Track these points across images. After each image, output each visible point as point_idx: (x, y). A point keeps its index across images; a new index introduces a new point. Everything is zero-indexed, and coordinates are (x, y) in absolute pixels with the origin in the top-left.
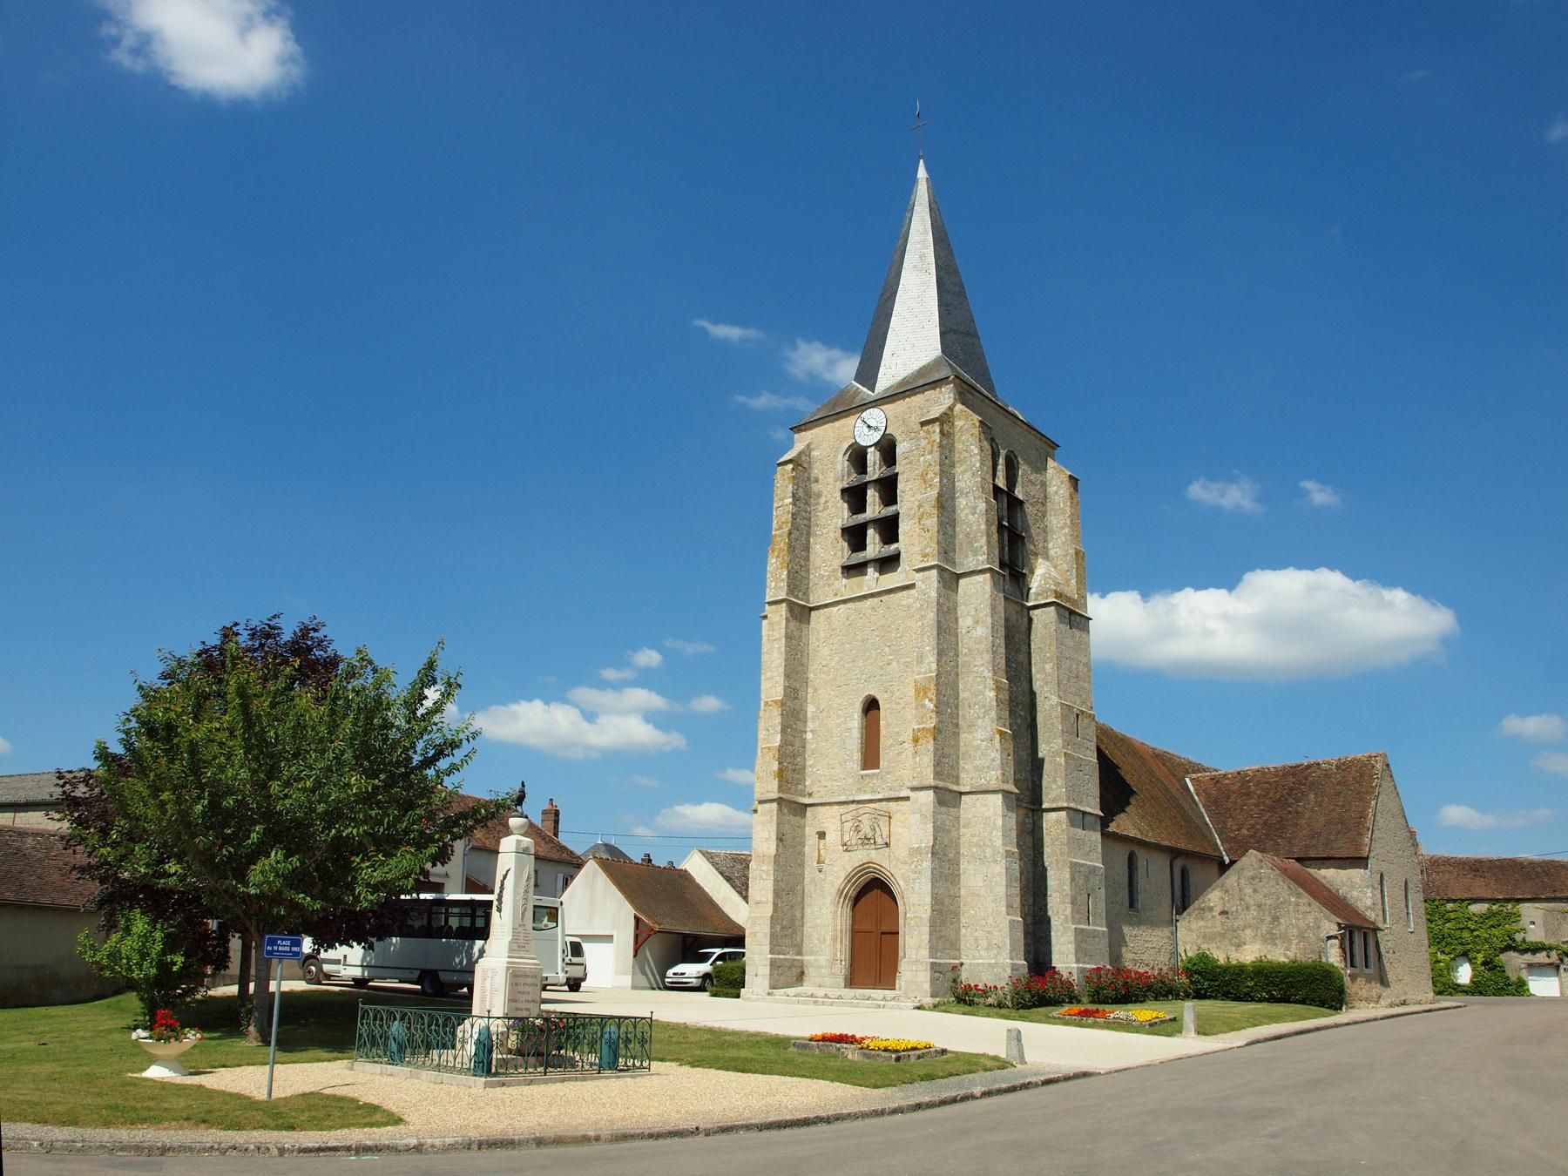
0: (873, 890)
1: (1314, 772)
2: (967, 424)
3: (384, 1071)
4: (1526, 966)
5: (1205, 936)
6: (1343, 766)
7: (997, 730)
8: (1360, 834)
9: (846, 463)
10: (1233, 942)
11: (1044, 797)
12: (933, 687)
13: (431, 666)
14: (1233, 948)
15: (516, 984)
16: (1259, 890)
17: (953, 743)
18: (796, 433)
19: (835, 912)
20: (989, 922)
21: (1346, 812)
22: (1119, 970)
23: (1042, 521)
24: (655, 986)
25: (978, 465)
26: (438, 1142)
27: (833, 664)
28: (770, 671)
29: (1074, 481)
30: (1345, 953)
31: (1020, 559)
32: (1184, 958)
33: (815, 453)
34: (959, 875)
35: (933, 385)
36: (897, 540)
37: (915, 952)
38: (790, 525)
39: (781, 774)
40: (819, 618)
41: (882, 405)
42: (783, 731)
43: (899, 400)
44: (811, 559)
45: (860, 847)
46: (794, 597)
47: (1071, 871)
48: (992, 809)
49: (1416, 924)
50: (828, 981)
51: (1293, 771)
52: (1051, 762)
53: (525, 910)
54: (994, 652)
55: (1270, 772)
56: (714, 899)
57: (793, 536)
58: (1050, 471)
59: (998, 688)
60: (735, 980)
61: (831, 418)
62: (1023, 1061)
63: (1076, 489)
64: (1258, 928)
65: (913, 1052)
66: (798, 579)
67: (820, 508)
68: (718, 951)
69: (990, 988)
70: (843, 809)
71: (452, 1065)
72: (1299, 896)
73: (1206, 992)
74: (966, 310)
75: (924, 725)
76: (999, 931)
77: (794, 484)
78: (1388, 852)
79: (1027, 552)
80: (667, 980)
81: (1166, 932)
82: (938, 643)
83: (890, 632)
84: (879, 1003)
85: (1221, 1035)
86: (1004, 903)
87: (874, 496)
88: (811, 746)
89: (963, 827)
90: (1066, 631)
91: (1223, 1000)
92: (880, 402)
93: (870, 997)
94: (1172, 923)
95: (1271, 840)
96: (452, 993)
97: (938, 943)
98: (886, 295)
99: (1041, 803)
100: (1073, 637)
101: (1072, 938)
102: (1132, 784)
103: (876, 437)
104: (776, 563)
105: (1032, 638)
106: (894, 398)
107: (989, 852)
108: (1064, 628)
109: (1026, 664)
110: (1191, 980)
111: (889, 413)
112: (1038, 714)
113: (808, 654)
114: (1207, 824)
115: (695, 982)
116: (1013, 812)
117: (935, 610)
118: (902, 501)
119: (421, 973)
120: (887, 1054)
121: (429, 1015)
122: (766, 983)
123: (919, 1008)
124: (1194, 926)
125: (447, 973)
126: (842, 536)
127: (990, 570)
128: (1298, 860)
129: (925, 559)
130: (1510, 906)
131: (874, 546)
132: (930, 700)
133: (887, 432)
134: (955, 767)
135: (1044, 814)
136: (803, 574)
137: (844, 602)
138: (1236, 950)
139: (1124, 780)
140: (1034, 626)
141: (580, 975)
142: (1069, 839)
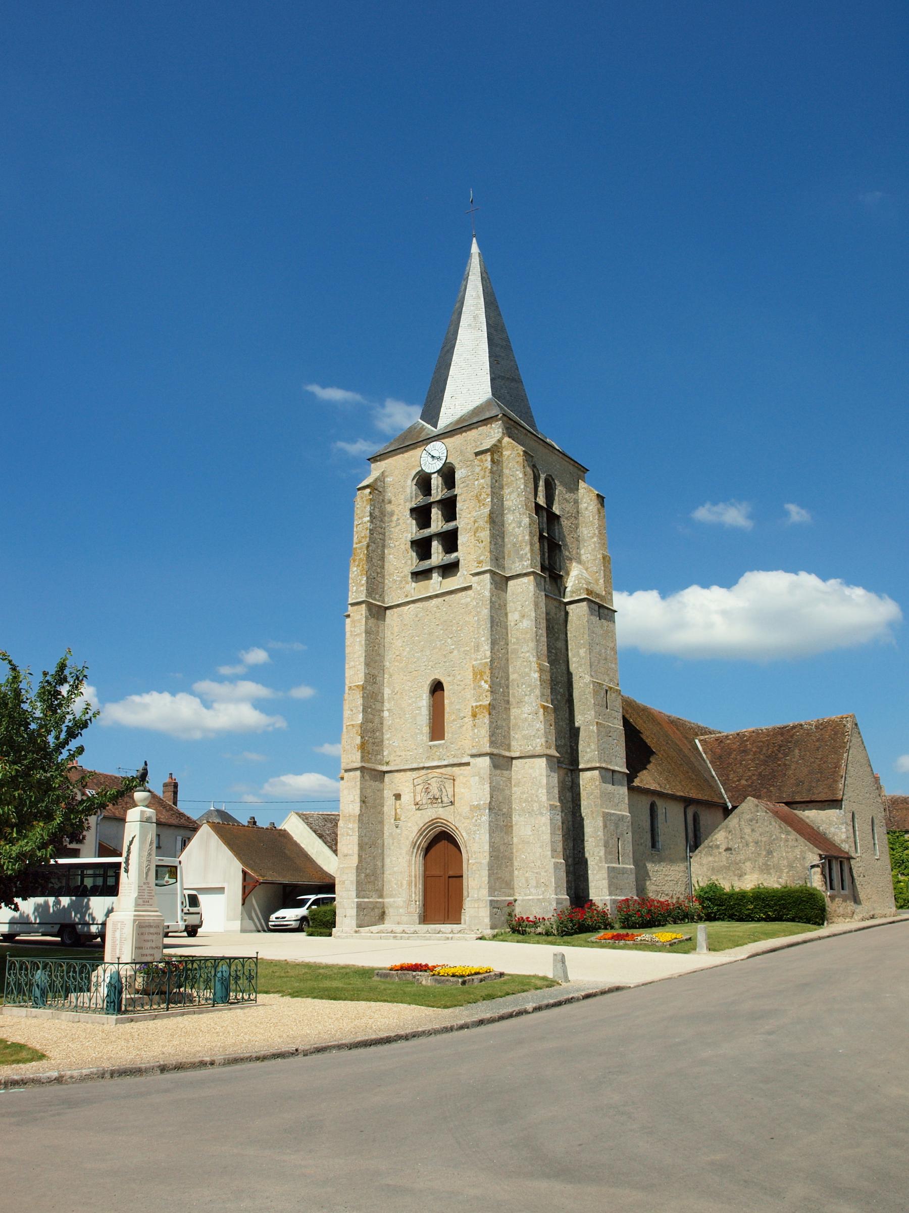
1: (798, 732)
2: (513, 453)
6: (821, 726)
8: (836, 781)
9: (414, 487)
10: (736, 872)
11: (580, 759)
12: (488, 672)
13: (62, 667)
14: (736, 878)
15: (142, 934)
16: (756, 829)
17: (505, 716)
19: (410, 861)
20: (537, 864)
22: (644, 900)
23: (576, 532)
24: (260, 929)
25: (522, 487)
26: (76, 1073)
27: (405, 653)
28: (353, 660)
29: (601, 498)
31: (558, 564)
32: (697, 888)
33: (389, 479)
34: (512, 826)
35: (485, 422)
38: (368, 539)
39: (363, 747)
41: (443, 438)
43: (457, 434)
44: (386, 567)
45: (430, 806)
46: (373, 599)
47: (604, 820)
48: (537, 771)
49: (881, 852)
50: (405, 919)
53: (149, 870)
54: (537, 641)
55: (763, 733)
57: (370, 548)
59: (541, 670)
60: (328, 921)
61: (401, 450)
62: (567, 980)
64: (756, 861)
65: (476, 977)
66: (375, 584)
67: (393, 524)
68: (313, 897)
69: (539, 919)
70: (415, 774)
72: (788, 833)
73: (715, 915)
74: (511, 360)
75: (481, 703)
76: (545, 872)
78: (858, 795)
81: (682, 866)
82: (491, 635)
86: (549, 848)
87: (437, 513)
88: (388, 722)
91: (729, 921)
93: (440, 931)
94: (687, 859)
97: (495, 883)
100: (602, 627)
101: (606, 875)
102: (652, 746)
103: (438, 465)
105: (568, 628)
106: (453, 433)
107: (536, 806)
108: (595, 619)
109: (563, 651)
110: (703, 906)
111: (450, 446)
112: (574, 690)
113: (384, 646)
114: (713, 777)
115: (294, 924)
116: (555, 772)
117: (489, 607)
118: (460, 518)
120: (455, 979)
122: (354, 923)
123: (480, 939)
124: (704, 861)
126: (412, 547)
127: (533, 573)
128: (787, 804)
129: (480, 565)
131: (438, 555)
132: (485, 682)
133: (447, 461)
134: (507, 736)
135: (581, 773)
136: (379, 579)
137: (413, 602)
138: (739, 879)
139: (645, 743)
140: (570, 618)
141: (197, 922)
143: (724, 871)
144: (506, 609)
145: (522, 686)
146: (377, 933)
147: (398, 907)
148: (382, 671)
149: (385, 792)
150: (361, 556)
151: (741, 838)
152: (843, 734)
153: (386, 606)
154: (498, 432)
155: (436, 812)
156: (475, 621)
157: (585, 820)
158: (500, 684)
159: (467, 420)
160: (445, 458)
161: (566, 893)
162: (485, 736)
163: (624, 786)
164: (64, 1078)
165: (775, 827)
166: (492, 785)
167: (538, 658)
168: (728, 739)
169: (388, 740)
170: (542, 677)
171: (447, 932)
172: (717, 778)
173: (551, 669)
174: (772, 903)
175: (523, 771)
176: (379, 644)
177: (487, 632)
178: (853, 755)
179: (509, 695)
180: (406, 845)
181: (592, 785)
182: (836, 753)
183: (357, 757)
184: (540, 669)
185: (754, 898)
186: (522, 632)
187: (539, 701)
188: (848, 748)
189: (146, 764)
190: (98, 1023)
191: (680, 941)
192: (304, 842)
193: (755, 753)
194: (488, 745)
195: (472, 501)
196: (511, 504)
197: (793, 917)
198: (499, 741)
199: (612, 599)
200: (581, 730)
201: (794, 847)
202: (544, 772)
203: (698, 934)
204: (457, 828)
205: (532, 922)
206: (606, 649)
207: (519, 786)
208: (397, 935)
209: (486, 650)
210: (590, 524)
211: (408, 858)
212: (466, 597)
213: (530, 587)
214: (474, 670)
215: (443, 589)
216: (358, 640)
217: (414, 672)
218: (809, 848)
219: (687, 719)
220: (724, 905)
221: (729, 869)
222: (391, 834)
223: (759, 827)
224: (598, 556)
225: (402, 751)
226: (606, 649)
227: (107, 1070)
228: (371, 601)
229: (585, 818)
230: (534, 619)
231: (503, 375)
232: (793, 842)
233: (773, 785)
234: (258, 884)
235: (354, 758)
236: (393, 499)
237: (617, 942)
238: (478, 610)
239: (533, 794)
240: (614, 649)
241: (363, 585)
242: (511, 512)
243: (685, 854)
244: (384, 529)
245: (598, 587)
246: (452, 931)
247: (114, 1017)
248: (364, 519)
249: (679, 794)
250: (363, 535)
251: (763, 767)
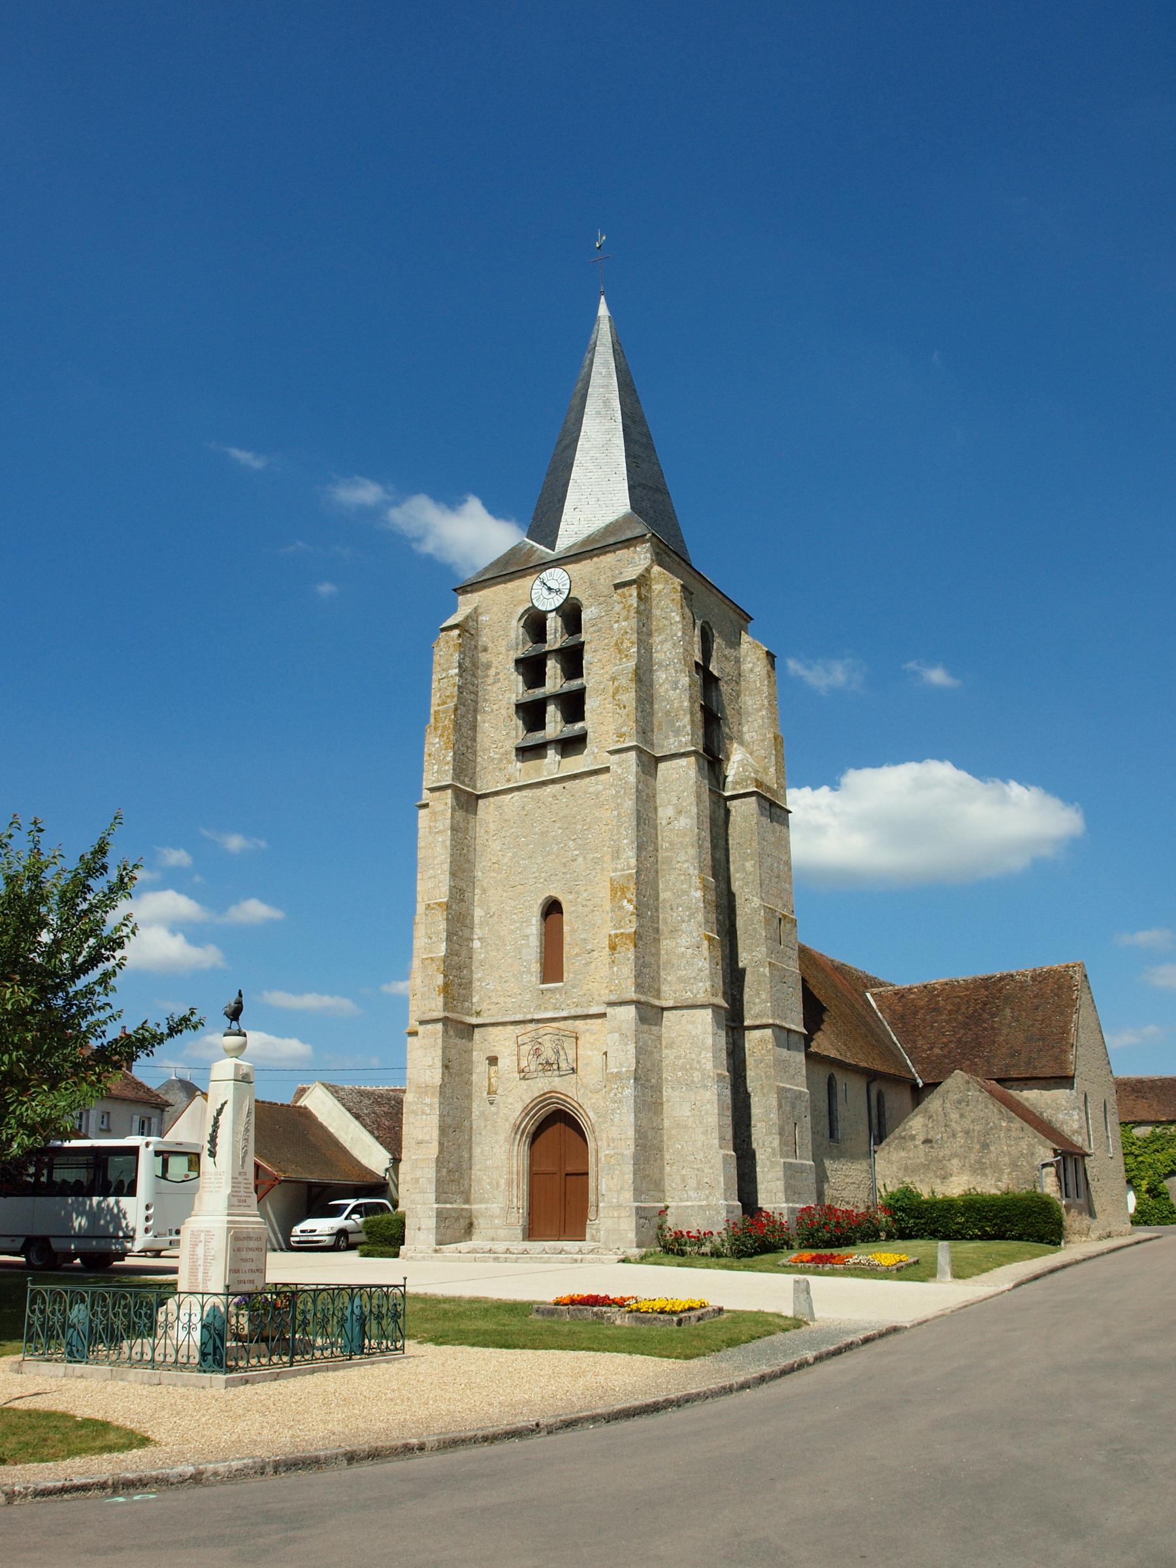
0: (555, 1123)
1: (1008, 985)
3: (70, 1371)
6: (1040, 978)
7: (705, 934)
9: (521, 630)
12: (632, 886)
13: (101, 850)
14: (939, 1181)
15: (239, 1250)
18: (460, 594)
19: (510, 1151)
20: (698, 1157)
21: (1047, 1027)
23: (737, 701)
24: (276, 1246)
25: (680, 634)
26: (221, 1467)
27: (506, 860)
28: (433, 868)
29: (770, 656)
30: (1060, 1182)
31: (716, 743)
32: (884, 1194)
33: (484, 618)
34: (662, 1104)
35: (626, 544)
37: (616, 1196)
38: (456, 699)
39: (446, 989)
41: (565, 564)
42: (449, 939)
43: (585, 559)
44: (478, 740)
45: (541, 1074)
46: (460, 783)
47: (778, 1097)
48: (699, 1027)
49: (1115, 1148)
50: (502, 1233)
51: (986, 983)
53: (246, 1153)
54: (700, 847)
55: (959, 986)
57: (459, 712)
58: (744, 646)
59: (705, 888)
60: (392, 1236)
61: (503, 578)
63: (773, 667)
64: (966, 1157)
65: (692, 1314)
66: (464, 763)
67: (490, 680)
68: (352, 1203)
69: (705, 1234)
70: (519, 1029)
71: (172, 1359)
72: (1010, 1120)
75: (622, 931)
78: (1089, 1071)
79: (723, 737)
80: (292, 1239)
81: (863, 1165)
83: (575, 823)
84: (575, 1256)
85: (975, 1278)
86: (716, 1134)
87: (555, 667)
88: (479, 956)
91: (931, 1239)
92: (560, 562)
93: (562, 1250)
94: (869, 1155)
95: (969, 1059)
96: (65, 1265)
98: (564, 443)
100: (774, 831)
101: (782, 1173)
102: (821, 999)
103: (558, 601)
104: (438, 743)
105: (729, 832)
106: (580, 557)
107: (697, 1076)
108: (766, 821)
110: (894, 1219)
111: (574, 574)
112: (738, 918)
113: (475, 849)
114: (895, 1044)
115: (328, 1241)
116: (723, 1030)
117: (634, 797)
118: (589, 674)
119: (26, 1240)
120: (666, 1317)
121: (114, 1294)
122: (432, 1238)
123: (623, 1261)
124: (894, 1157)
125: (62, 1240)
126: (517, 712)
128: (999, 1081)
129: (622, 739)
131: (554, 725)
132: (629, 901)
133: (571, 596)
134: (656, 978)
135: (746, 1032)
136: (470, 756)
138: (942, 1182)
140: (732, 818)
143: (922, 1171)
145: (677, 908)
146: (468, 1253)
147: (492, 1217)
148: (471, 884)
149: (474, 1053)
150: (446, 722)
151: (946, 1126)
152: (1070, 988)
153: (480, 793)
154: (645, 558)
155: (550, 1083)
156: (614, 817)
157: (752, 1097)
158: (648, 905)
159: (598, 541)
160: (568, 591)
161: (737, 1198)
162: (629, 977)
164: (204, 1476)
165: (993, 1112)
167: (701, 871)
168: (911, 993)
170: (706, 897)
171: (573, 1251)
172: (899, 1045)
173: (717, 887)
175: (678, 1027)
176: (468, 846)
180: (505, 1128)
181: (763, 1050)
182: (1062, 1014)
183: (438, 1003)
184: (704, 886)
187: (702, 930)
189: (240, 995)
190: (194, 1386)
191: (909, 1265)
192: (334, 1124)
193: (950, 1012)
194: (633, 989)
195: (606, 651)
197: (1019, 1234)
200: (747, 972)
201: (1019, 1138)
202: (710, 1030)
203: (939, 1254)
204: (580, 1106)
205: (694, 1237)
206: (779, 862)
207: (672, 1048)
208: (499, 1255)
209: (629, 857)
212: (597, 784)
214: (612, 885)
215: (562, 772)
216: (440, 839)
217: (519, 887)
218: (1039, 1140)
219: (854, 966)
221: (929, 1169)
222: (483, 1113)
223: (971, 1111)
224: (768, 736)
226: (779, 862)
227: (269, 1462)
228: (459, 785)
229: (752, 1094)
230: (696, 816)
231: (644, 482)
232: (1018, 1132)
234: (277, 1182)
235: (434, 1006)
236: (490, 645)
237: (820, 1265)
239: (693, 1060)
240: (788, 863)
241: (448, 763)
242: (664, 669)
243: (867, 1149)
244: (477, 687)
246: (580, 1251)
247: (224, 1377)
248: (450, 671)
251: (962, 1031)
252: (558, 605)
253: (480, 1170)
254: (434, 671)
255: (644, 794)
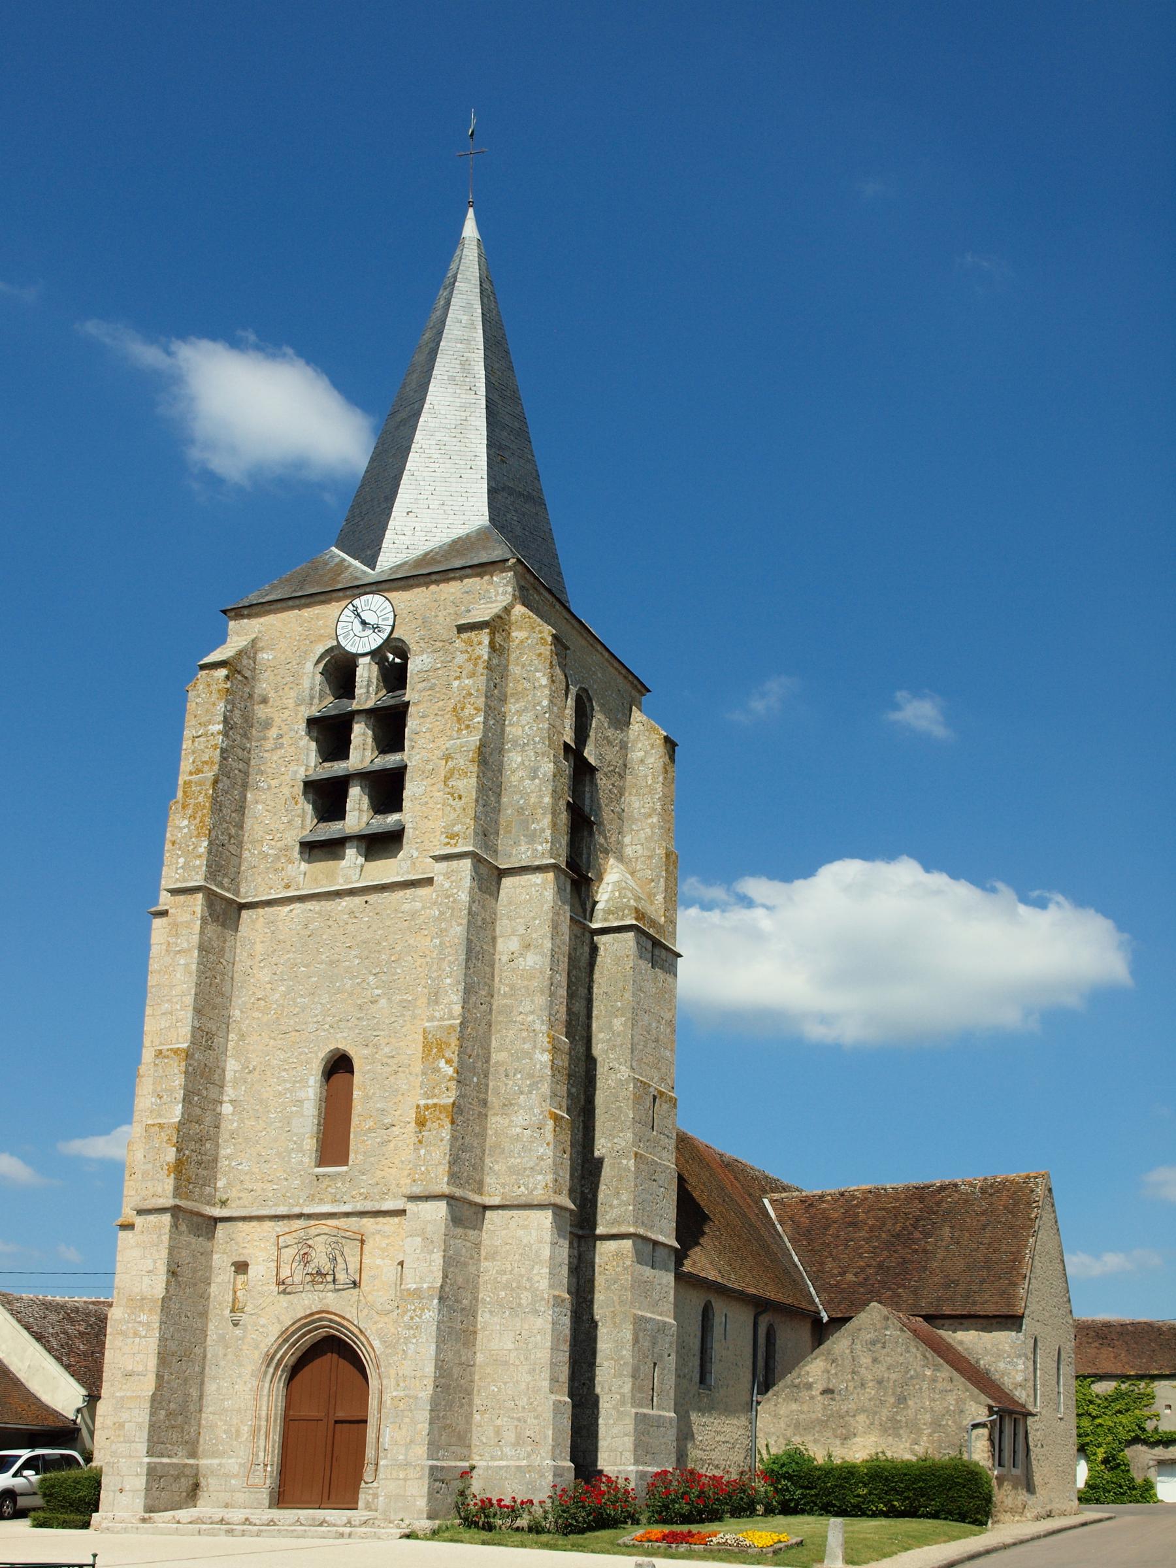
4: (1155, 1463)
5: (797, 1425)
6: (991, 1190)
7: (551, 1113)
8: (1014, 1284)
9: (319, 678)
10: (839, 1432)
11: (599, 1217)
12: (454, 1042)
14: (838, 1442)
17: (477, 1129)
18: (231, 619)
19: (259, 1389)
20: (520, 1404)
22: (693, 1477)
25: (545, 703)
27: (277, 996)
31: (584, 856)
32: (765, 1456)
33: (265, 656)
34: (475, 1332)
35: (479, 570)
36: (398, 808)
38: (216, 767)
39: (179, 1168)
40: (253, 921)
41: (388, 590)
42: (187, 1099)
43: (418, 586)
44: (247, 827)
45: (308, 1287)
46: (217, 886)
48: (534, 1233)
50: (240, 1497)
51: (921, 1193)
52: (612, 1166)
55: (887, 1195)
56: (12, 1368)
57: (220, 785)
59: (555, 1049)
60: (81, 1499)
61: (297, 602)
64: (875, 1413)
67: (269, 745)
68: (25, 1454)
70: (281, 1227)
72: (937, 1368)
73: (797, 1505)
74: (528, 461)
75: (435, 1101)
77: (227, 702)
81: (743, 1421)
82: (465, 975)
86: (546, 1374)
89: (485, 1259)
90: (646, 970)
91: (821, 1515)
92: (381, 587)
94: (751, 1407)
95: (889, 1289)
99: (594, 1226)
101: (631, 1428)
103: (375, 641)
105: (595, 977)
106: (411, 582)
107: (526, 1298)
108: (645, 966)
109: (583, 1018)
110: (776, 1488)
111: (401, 607)
114: (796, 1266)
116: (565, 1239)
117: (465, 922)
118: (413, 747)
122: (139, 1503)
123: (408, 1536)
124: (783, 1410)
126: (305, 793)
128: (927, 1318)
129: (453, 842)
130: (1142, 1384)
133: (395, 635)
134: (478, 1167)
135: (598, 1243)
136: (233, 849)
138: (842, 1444)
140: (599, 959)
142: (634, 1280)
143: (817, 1429)
144: (494, 930)
145: (515, 1075)
146: (190, 1523)
148: (224, 1026)
149: (215, 1257)
150: (201, 799)
151: (853, 1372)
152: (1029, 1204)
155: (321, 1300)
156: (435, 947)
159: (440, 562)
160: (390, 628)
163: (670, 1271)
165: (916, 1357)
166: (448, 1254)
168: (823, 1202)
169: (227, 1158)
171: (339, 1522)
172: (801, 1268)
174: (902, 1485)
175: (504, 1232)
177: (458, 970)
178: (1040, 1243)
179: (487, 1090)
181: (618, 1266)
183: (166, 1187)
185: (870, 1477)
186: (522, 976)
187: (547, 1106)
188: (1036, 1229)
193: (871, 1229)
195: (439, 718)
196: (520, 733)
198: (465, 1174)
199: (675, 933)
205: (507, 1507)
207: (494, 1259)
208: (235, 1527)
209: (453, 1002)
210: (648, 789)
211: (255, 1383)
212: (413, 900)
213: (546, 893)
214: (425, 1038)
216: (182, 962)
217: (294, 1033)
218: (971, 1395)
220: (816, 1488)
222: (222, 1338)
224: (658, 852)
225: (257, 1181)
228: (214, 888)
233: (904, 1285)
236: (272, 694)
237: (674, 1546)
238: (443, 925)
239: (522, 1276)
241: (200, 856)
242: (519, 749)
244: (249, 752)
245: (653, 908)
246: (349, 1522)
248: (210, 727)
249: (751, 1291)
250: (206, 758)
252: (374, 646)
253: (214, 1414)
254: (186, 724)
255: (479, 918)
